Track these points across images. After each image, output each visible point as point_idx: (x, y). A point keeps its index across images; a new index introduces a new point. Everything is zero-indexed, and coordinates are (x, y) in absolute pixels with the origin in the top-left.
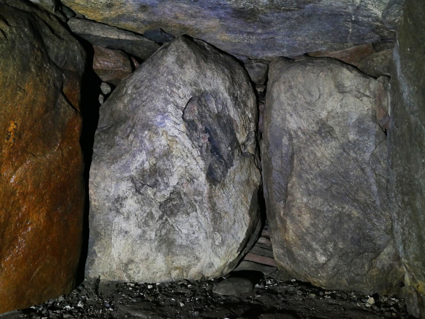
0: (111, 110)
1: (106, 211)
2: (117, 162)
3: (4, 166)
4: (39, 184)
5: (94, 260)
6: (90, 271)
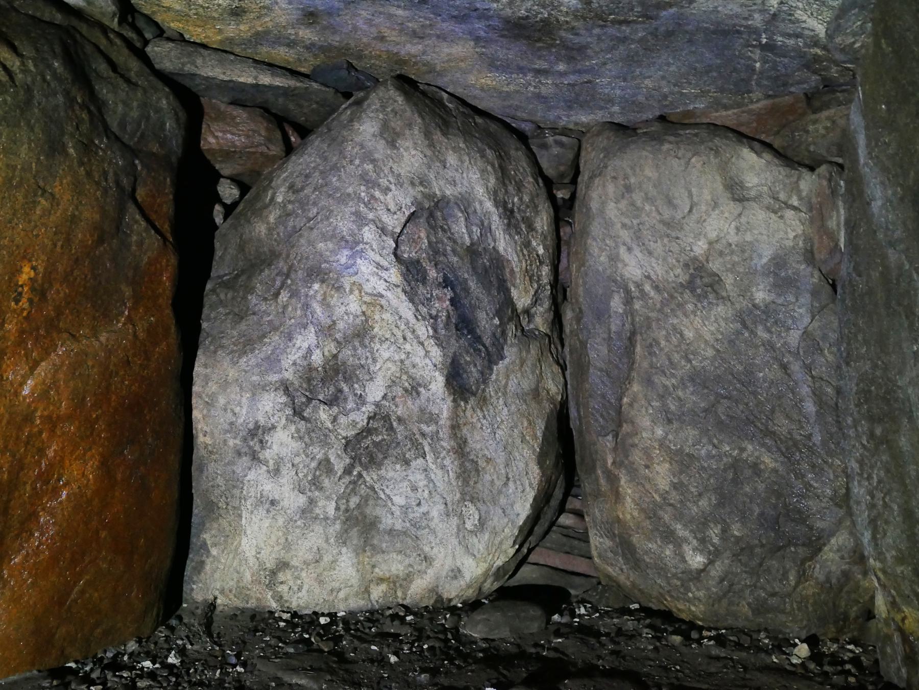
0: (241, 238)
1: (230, 456)
2: (252, 351)
3: (9, 359)
4: (84, 398)
5: (202, 563)
6: (194, 587)
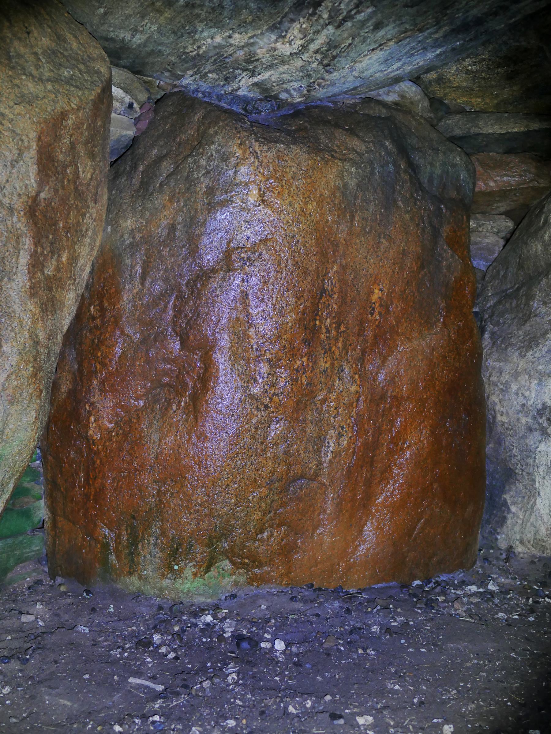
0: (520, 258)
1: (522, 432)
2: (537, 346)
3: (369, 355)
4: (418, 383)
5: (504, 519)
6: (499, 537)
